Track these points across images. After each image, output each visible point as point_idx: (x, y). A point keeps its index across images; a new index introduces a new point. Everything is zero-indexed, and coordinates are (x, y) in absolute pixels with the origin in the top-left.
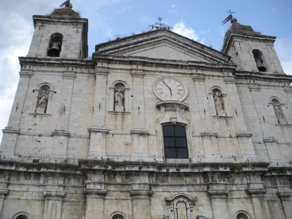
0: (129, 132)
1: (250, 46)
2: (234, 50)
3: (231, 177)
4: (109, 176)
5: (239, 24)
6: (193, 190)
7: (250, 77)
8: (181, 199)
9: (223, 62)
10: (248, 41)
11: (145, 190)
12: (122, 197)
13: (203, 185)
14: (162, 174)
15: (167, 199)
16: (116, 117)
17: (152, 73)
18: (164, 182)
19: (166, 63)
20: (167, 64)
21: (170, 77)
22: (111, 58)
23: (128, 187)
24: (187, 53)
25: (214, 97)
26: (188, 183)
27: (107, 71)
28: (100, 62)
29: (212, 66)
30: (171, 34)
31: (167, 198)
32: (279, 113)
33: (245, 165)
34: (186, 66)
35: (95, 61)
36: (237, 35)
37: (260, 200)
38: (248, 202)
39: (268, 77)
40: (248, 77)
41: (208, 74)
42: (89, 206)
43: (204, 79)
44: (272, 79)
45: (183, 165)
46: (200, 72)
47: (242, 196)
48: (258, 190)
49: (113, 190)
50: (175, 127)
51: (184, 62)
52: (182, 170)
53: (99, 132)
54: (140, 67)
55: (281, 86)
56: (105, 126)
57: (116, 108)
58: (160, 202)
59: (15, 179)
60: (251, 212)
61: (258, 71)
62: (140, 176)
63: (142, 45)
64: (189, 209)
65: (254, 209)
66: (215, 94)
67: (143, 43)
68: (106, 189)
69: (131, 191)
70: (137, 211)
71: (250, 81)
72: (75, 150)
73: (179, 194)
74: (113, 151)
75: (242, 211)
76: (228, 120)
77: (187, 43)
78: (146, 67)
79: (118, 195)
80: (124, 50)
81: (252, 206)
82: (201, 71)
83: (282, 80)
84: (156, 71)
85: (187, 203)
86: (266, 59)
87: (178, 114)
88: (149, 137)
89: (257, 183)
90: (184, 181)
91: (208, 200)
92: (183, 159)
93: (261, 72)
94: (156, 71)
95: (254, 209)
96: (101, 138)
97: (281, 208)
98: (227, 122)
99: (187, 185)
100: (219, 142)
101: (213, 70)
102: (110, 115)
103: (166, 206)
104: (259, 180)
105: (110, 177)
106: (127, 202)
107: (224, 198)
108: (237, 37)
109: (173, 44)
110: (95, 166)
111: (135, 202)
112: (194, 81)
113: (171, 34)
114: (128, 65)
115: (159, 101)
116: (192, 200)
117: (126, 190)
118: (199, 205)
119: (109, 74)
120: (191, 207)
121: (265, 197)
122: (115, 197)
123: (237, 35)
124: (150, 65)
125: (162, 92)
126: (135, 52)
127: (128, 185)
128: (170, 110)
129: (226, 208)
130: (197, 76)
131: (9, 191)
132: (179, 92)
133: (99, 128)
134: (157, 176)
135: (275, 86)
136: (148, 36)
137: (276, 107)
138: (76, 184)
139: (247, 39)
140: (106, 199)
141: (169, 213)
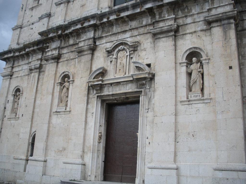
6: (137, 34)
8: (121, 47)
11: (87, 45)
37: (224, 29)
38: (207, 34)
45: (122, 8)
48: (220, 15)
49: (66, 52)
52: (123, 14)
59: (17, 62)
62: (87, 33)
64: (128, 56)
75: (195, 48)
89: (222, 6)
110: (50, 34)
131: (13, 72)
134: (103, 28)
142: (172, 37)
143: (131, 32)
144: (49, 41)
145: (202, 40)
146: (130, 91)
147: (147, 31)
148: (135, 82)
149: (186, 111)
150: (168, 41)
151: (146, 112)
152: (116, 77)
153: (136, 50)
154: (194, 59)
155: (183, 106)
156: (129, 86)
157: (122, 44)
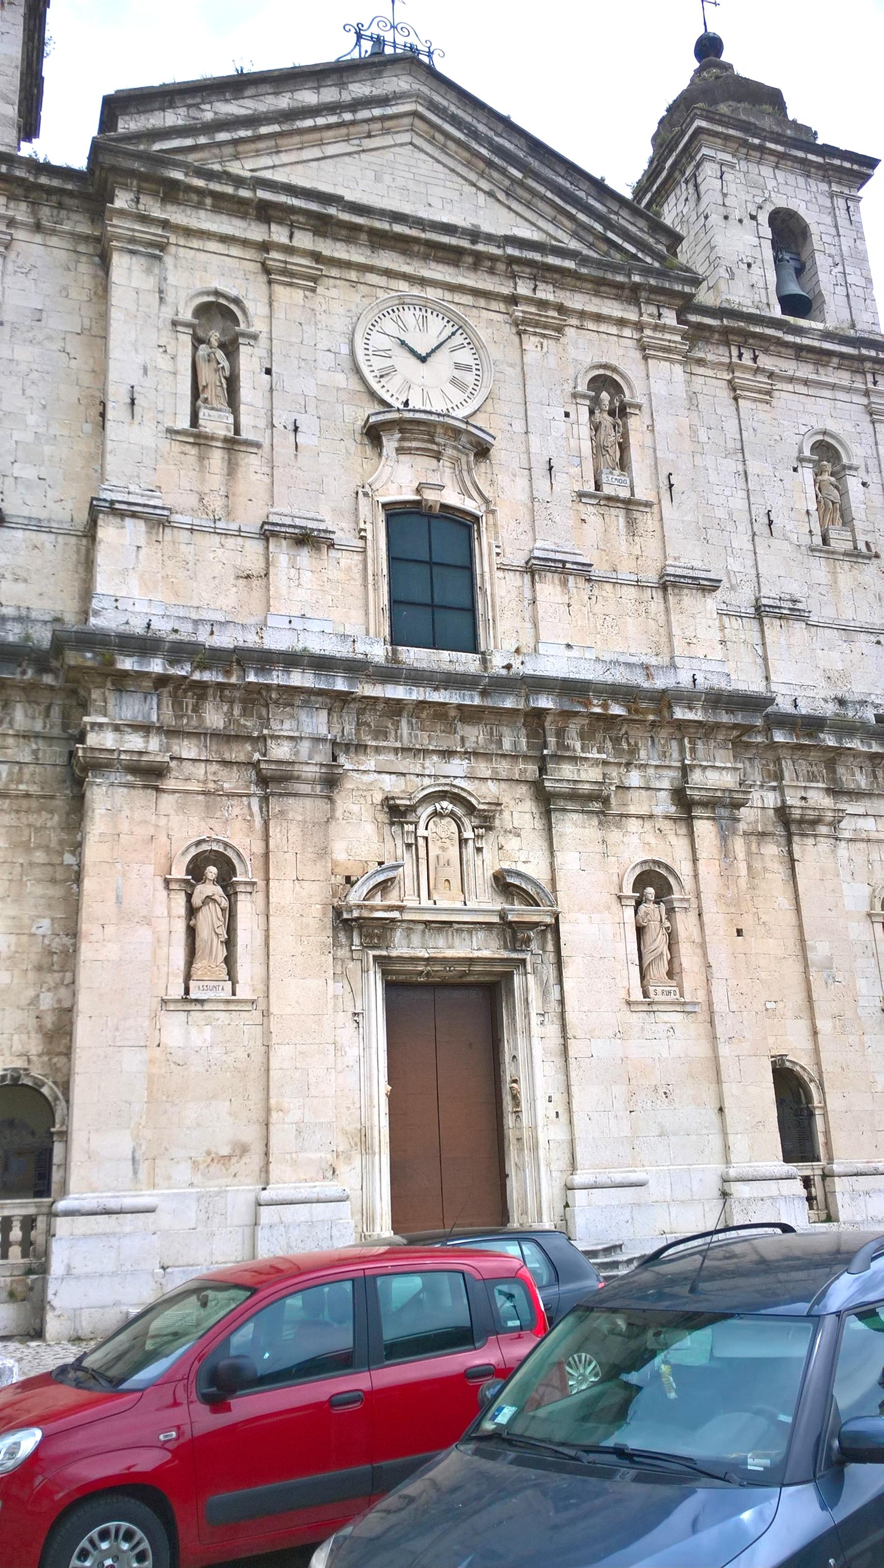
0: (253, 526)
1: (764, 188)
2: (693, 198)
3: (627, 739)
4: (177, 704)
5: (728, 67)
6: (488, 774)
7: (744, 339)
8: (445, 804)
9: (649, 260)
10: (759, 163)
12: (226, 785)
13: (525, 757)
14: (380, 706)
15: (391, 802)
16: (201, 458)
17: (353, 275)
18: (386, 735)
19: (414, 233)
20: (416, 240)
21: (424, 305)
22: (177, 175)
23: (248, 747)
24: (501, 196)
25: (592, 412)
26: (470, 745)
27: (159, 239)
28: (126, 187)
29: (600, 273)
30: (443, 89)
31: (393, 798)
32: (833, 503)
33: (688, 698)
34: (493, 259)
35: (106, 182)
36: (720, 129)
38: (679, 832)
39: (816, 344)
40: (736, 338)
41: (578, 306)
42: (97, 817)
43: (559, 329)
44: (830, 353)
46: (545, 293)
47: (658, 811)
48: (719, 794)
50: (434, 522)
51: (490, 238)
53: (134, 515)
54: (304, 240)
55: (857, 390)
56: (157, 494)
57: (201, 415)
60: (684, 868)
61: (776, 312)
63: (315, 129)
64: (471, 843)
65: (695, 860)
66: (595, 402)
67: (321, 121)
68: (168, 751)
69: (263, 766)
71: (740, 356)
72: (25, 581)
73: (439, 785)
74: (191, 598)
75: (655, 862)
76: (636, 515)
77: (507, 144)
78: (329, 242)
79: (210, 777)
80: (235, 142)
81: (689, 848)
82: (550, 288)
83: (868, 365)
84: (370, 269)
85: (466, 820)
86: (819, 258)
87: (448, 470)
91: (537, 816)
93: (791, 319)
94: (370, 269)
95: (695, 860)
97: (787, 859)
98: (631, 523)
99: (466, 753)
100: (594, 598)
101: (603, 289)
102: (176, 447)
103: (387, 828)
104: (723, 758)
105: (180, 704)
107: (597, 813)
108: (719, 141)
109: (450, 144)
112: (519, 334)
113: (442, 92)
114: (253, 224)
115: (378, 408)
116: (484, 810)
117: (242, 758)
118: (505, 831)
119: (167, 254)
120: (479, 837)
121: (738, 820)
122: (201, 785)
123: (720, 129)
124: (344, 232)
126: (285, 158)
127: (249, 738)
128: (417, 449)
129: (600, 848)
130: (533, 310)
132: (458, 374)
133: (132, 499)
135: (834, 387)
136: (342, 85)
137: (826, 477)
138: (38, 726)
139: (758, 155)
140: (164, 791)
141: (399, 852)
146: (486, 953)
157: (442, 795)
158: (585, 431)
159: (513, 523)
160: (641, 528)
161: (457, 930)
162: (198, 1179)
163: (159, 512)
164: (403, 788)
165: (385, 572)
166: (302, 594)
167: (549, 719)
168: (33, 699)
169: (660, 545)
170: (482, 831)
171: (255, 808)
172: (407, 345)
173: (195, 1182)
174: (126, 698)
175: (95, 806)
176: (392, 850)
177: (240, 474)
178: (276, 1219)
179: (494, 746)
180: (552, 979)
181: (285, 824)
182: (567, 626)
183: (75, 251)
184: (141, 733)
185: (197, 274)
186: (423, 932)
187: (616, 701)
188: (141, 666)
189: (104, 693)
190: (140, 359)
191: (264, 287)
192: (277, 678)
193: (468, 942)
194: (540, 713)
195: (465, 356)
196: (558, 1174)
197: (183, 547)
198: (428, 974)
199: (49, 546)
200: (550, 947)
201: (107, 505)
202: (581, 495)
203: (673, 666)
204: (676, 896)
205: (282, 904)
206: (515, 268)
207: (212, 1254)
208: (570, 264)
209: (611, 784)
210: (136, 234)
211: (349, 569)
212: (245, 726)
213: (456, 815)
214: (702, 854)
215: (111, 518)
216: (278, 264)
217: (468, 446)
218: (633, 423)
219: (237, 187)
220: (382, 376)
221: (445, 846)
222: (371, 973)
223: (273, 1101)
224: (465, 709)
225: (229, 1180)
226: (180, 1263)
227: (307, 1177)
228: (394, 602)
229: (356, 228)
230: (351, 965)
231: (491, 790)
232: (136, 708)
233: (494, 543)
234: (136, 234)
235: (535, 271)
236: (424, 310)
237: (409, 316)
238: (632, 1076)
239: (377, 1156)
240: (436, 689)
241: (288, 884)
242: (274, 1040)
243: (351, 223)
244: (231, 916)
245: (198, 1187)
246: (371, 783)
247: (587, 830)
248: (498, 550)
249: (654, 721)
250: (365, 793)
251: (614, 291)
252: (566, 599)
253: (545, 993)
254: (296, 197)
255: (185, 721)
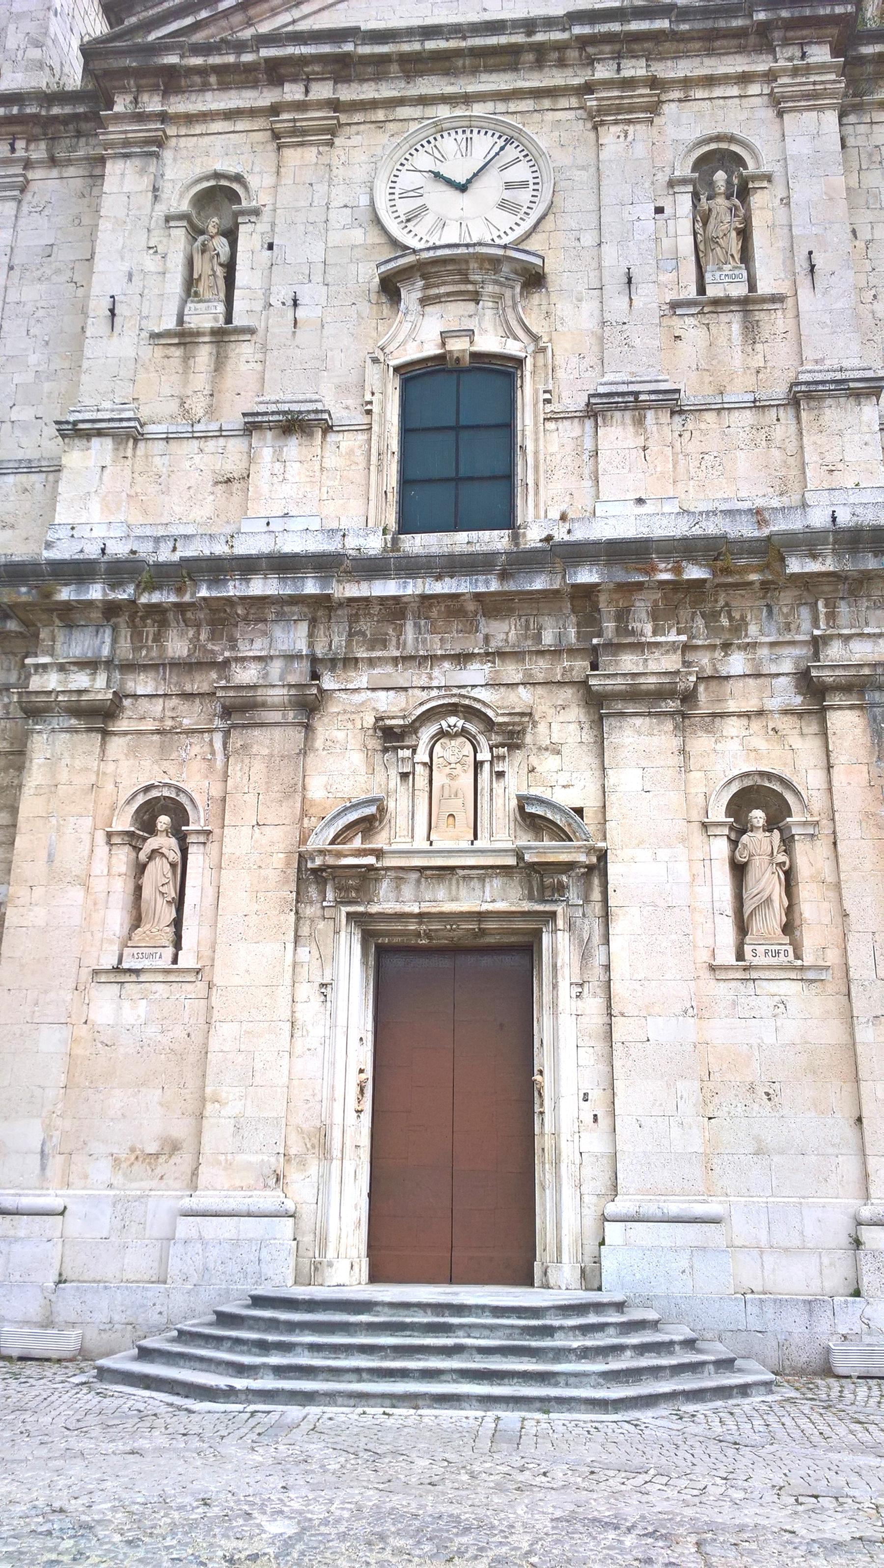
0: (238, 422)
3: (729, 613)
4: (137, 635)
6: (518, 678)
8: (452, 720)
12: (186, 721)
14: (376, 609)
17: (380, 115)
18: (384, 644)
19: (453, 44)
20: (458, 53)
21: (469, 126)
22: (172, 59)
23: (214, 675)
28: (124, 90)
29: (709, 24)
34: (560, 47)
38: (806, 730)
42: (35, 767)
46: (635, 69)
47: (773, 704)
48: (866, 671)
49: (149, 690)
51: (550, 23)
53: (100, 433)
54: (322, 91)
58: (354, 737)
64: (487, 766)
70: (245, 781)
72: (13, 527)
74: (162, 515)
75: (762, 774)
78: (355, 85)
84: (401, 102)
85: (482, 739)
88: (332, 438)
90: (480, 636)
91: (586, 726)
92: (481, 533)
94: (401, 102)
96: (108, 462)
98: (751, 331)
100: (687, 435)
101: (718, 44)
102: (159, 352)
103: (378, 756)
105: (140, 634)
106: (207, 740)
107: (671, 714)
111: (237, 739)
114: (265, 90)
117: (205, 688)
118: (540, 749)
122: (157, 723)
125: (424, 208)
127: (213, 664)
128: (448, 294)
129: (678, 760)
132: (508, 195)
133: (100, 416)
141: (392, 785)
142: (674, 719)
143: (490, 665)
144: (44, 617)
145: (787, 747)
146: (501, 906)
147: (563, 675)
148: (521, 873)
149: (734, 1004)
150: (655, 732)
151: (574, 996)
152: (437, 846)
153: (518, 747)
154: (758, 816)
155: (721, 984)
156: (492, 886)
157: (453, 709)
158: (685, 225)
159: (575, 360)
160: (765, 331)
161: (464, 877)
162: (118, 1180)
163: (125, 424)
164: (403, 705)
165: (395, 446)
166: (286, 490)
167: (603, 599)
168: (8, 650)
169: (796, 348)
170: (503, 751)
171: (218, 745)
172: (442, 177)
173: (115, 1182)
174: (77, 635)
175: (34, 755)
176: (383, 781)
177: (229, 367)
178: (194, 1234)
179: (530, 642)
180: (597, 939)
181: (247, 761)
182: (641, 476)
183: (91, 176)
184: (88, 671)
185: (198, 161)
186: (418, 881)
187: (693, 560)
188: (78, 594)
189: (53, 632)
190: (125, 267)
191: (273, 155)
192: (233, 589)
193: (478, 892)
194: (588, 592)
195: (521, 172)
196: (594, 1199)
197: (157, 460)
198: (428, 935)
199: (39, 487)
200: (596, 895)
201: (70, 427)
202: (675, 305)
203: (804, 505)
204: (796, 817)
205: (238, 854)
206: (590, 50)
207: (122, 1270)
208: (663, 24)
209: (690, 673)
210: (129, 135)
211: (351, 452)
212: (212, 651)
213: (470, 734)
214: (840, 759)
215: (76, 441)
216: (286, 125)
217: (512, 276)
218: (757, 200)
219: (239, 54)
220: (408, 221)
221: (455, 772)
222: (343, 934)
223: (208, 1090)
224: (487, 600)
225: (154, 1183)
226: (86, 1278)
227: (244, 1184)
228: (405, 482)
229: (383, 60)
230: (321, 925)
231: (523, 697)
232: (87, 643)
233: (541, 388)
234: (129, 135)
235: (617, 47)
236: (468, 131)
237: (449, 144)
238: (714, 1068)
239: (336, 1163)
240: (439, 578)
241: (247, 830)
242: (216, 1015)
243: (373, 55)
244: (181, 869)
245: (118, 1189)
246: (362, 704)
247: (655, 739)
248: (548, 396)
249: (763, 583)
250: (353, 717)
251: (734, 42)
252: (641, 441)
253: (585, 956)
254: (306, 44)
255: (144, 653)
